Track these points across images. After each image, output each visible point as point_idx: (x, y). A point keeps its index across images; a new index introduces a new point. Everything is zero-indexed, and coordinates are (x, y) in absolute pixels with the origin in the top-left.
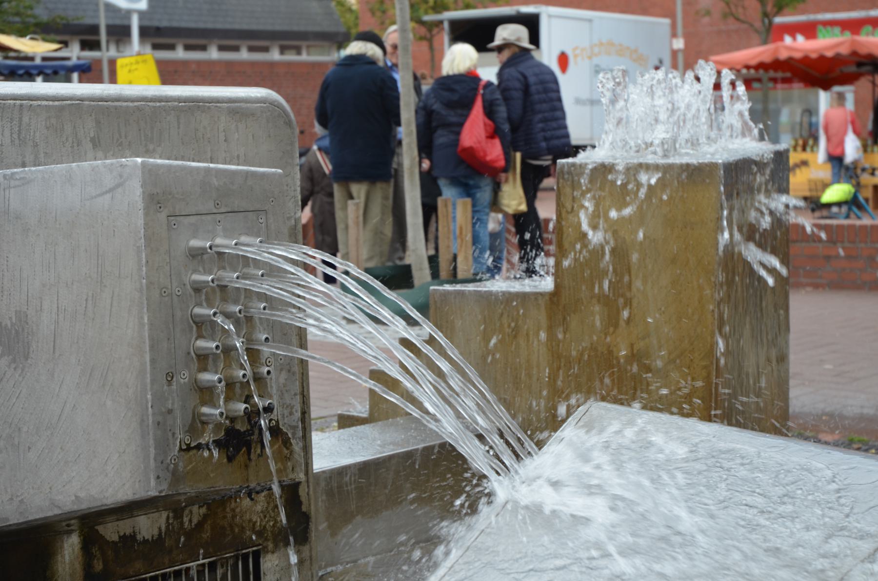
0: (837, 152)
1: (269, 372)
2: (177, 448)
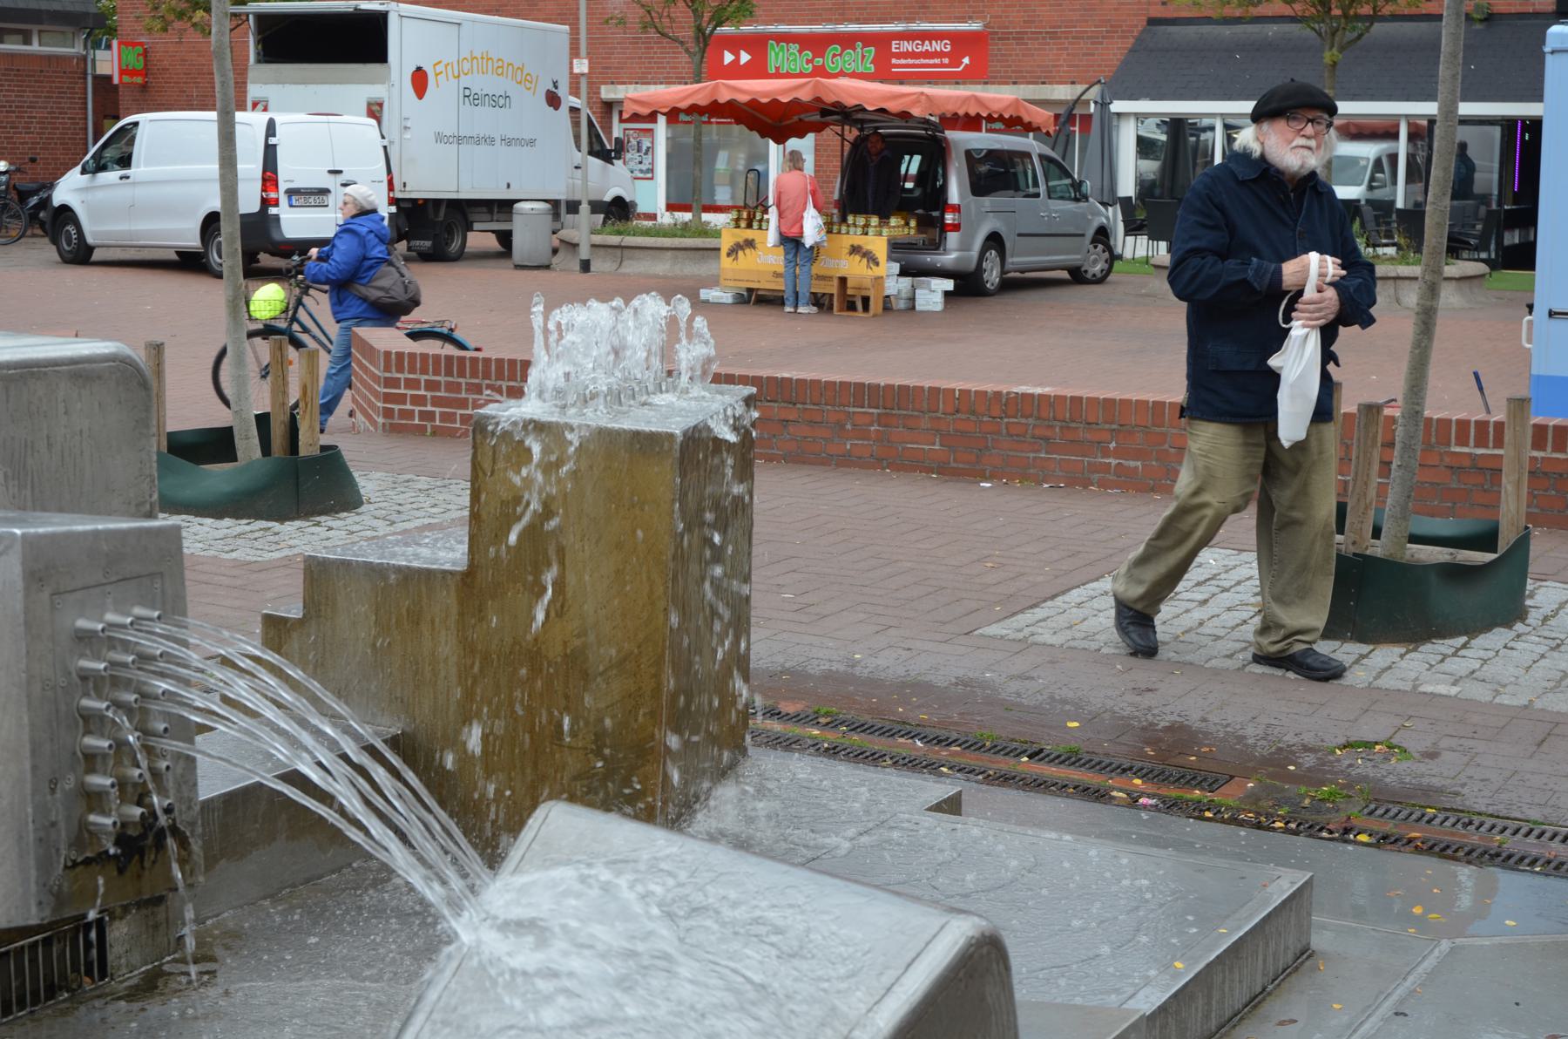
0: (793, 232)
1: (168, 768)
2: (62, 866)
